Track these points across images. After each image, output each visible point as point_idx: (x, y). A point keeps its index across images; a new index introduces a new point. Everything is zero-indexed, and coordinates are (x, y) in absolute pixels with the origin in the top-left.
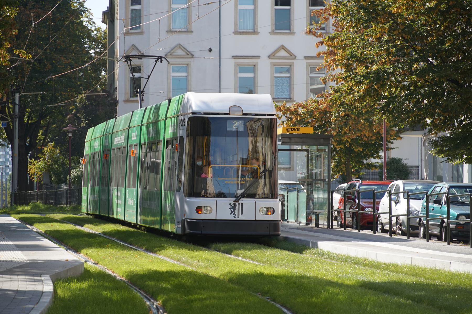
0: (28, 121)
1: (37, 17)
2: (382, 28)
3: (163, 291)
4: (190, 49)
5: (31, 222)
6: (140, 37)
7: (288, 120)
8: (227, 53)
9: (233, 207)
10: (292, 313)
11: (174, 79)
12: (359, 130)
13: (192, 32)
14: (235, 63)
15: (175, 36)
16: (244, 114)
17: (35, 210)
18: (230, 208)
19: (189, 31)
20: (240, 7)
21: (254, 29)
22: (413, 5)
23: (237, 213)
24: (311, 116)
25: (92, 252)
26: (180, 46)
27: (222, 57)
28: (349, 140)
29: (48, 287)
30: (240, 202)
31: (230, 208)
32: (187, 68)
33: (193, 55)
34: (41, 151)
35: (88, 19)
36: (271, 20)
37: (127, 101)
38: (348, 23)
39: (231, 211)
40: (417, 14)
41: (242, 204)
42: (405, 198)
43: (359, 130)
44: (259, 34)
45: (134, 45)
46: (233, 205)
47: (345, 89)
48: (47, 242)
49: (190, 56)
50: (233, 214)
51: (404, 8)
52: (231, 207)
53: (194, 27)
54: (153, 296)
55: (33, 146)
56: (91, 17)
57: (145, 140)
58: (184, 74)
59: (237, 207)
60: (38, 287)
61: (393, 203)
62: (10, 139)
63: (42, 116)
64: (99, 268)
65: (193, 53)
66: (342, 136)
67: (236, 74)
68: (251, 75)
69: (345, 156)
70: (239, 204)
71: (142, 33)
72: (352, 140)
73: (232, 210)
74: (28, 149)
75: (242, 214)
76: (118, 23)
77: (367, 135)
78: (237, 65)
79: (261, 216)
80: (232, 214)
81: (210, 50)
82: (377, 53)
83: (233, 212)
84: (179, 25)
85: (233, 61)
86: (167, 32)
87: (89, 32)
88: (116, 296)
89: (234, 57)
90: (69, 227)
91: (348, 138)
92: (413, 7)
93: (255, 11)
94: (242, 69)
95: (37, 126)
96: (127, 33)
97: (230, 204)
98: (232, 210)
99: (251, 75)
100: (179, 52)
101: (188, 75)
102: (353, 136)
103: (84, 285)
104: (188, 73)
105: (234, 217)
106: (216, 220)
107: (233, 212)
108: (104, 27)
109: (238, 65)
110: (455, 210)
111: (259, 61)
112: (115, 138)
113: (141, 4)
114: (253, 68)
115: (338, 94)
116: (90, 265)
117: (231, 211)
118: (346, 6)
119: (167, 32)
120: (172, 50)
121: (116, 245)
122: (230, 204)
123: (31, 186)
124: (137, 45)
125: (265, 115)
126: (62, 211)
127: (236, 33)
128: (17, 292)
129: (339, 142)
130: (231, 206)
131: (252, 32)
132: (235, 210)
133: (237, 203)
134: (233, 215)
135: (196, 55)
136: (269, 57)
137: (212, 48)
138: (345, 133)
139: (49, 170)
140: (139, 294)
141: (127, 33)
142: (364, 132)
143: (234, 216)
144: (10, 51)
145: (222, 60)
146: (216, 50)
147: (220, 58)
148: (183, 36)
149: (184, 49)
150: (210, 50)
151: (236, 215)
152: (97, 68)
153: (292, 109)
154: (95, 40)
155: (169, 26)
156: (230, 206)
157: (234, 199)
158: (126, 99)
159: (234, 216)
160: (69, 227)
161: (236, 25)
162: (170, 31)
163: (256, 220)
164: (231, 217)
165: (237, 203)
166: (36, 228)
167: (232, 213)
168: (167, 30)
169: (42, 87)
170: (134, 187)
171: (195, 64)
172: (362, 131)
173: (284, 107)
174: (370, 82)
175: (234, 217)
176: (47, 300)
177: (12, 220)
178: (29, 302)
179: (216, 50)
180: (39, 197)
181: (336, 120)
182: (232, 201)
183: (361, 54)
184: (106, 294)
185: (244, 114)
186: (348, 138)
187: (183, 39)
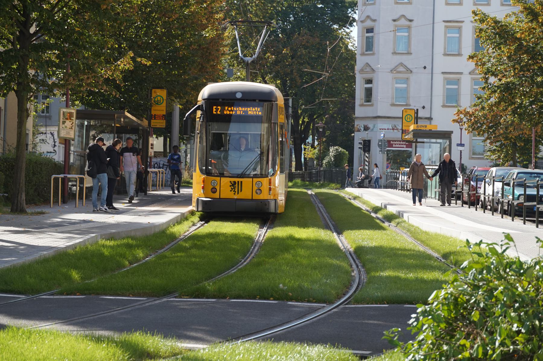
0: (316, 118)
1: (331, 43)
2: (509, 49)
4: (409, 66)
6: (372, 57)
7: (468, 121)
8: (437, 70)
11: (397, 89)
12: (521, 129)
13: (411, 54)
14: (444, 77)
15: (398, 57)
18: (230, 186)
19: (409, 53)
20: (448, 35)
21: (459, 52)
22: (534, 32)
23: (236, 190)
24: (485, 118)
26: (401, 64)
27: (434, 72)
28: (513, 137)
31: (230, 186)
32: (406, 81)
33: (411, 71)
35: (352, 45)
36: (472, 46)
37: (362, 105)
38: (488, 45)
40: (537, 38)
43: (521, 129)
44: (463, 56)
45: (367, 63)
47: (485, 96)
49: (409, 72)
51: (527, 34)
53: (413, 49)
56: (354, 43)
58: (405, 86)
59: (237, 185)
61: (487, 185)
65: (411, 69)
66: (508, 134)
67: (444, 86)
68: (456, 87)
69: (512, 149)
71: (373, 54)
72: (515, 137)
73: (232, 187)
75: (241, 191)
77: (527, 132)
78: (445, 79)
81: (425, 68)
82: (505, 68)
84: (401, 48)
85: (442, 76)
86: (392, 53)
89: (443, 73)
91: (513, 135)
92: (534, 33)
93: (460, 39)
94: (449, 82)
98: (232, 187)
99: (456, 87)
100: (401, 69)
101: (408, 86)
102: (516, 133)
104: (408, 85)
109: (446, 79)
110: (517, 191)
111: (462, 76)
114: (457, 82)
115: (480, 100)
118: (487, 32)
119: (392, 53)
120: (396, 67)
122: (230, 182)
124: (369, 63)
127: (445, 55)
129: (506, 138)
130: (231, 183)
131: (457, 54)
135: (414, 71)
136: (470, 73)
138: (511, 131)
142: (525, 131)
145: (434, 75)
146: (429, 68)
147: (432, 73)
148: (404, 57)
149: (405, 67)
150: (425, 68)
151: (235, 192)
153: (471, 113)
155: (394, 49)
156: (230, 184)
158: (361, 103)
161: (445, 48)
162: (394, 53)
168: (392, 52)
171: (413, 78)
172: (524, 130)
173: (465, 111)
174: (501, 91)
179: (429, 68)
181: (504, 122)
183: (495, 69)
186: (513, 135)
187: (404, 59)
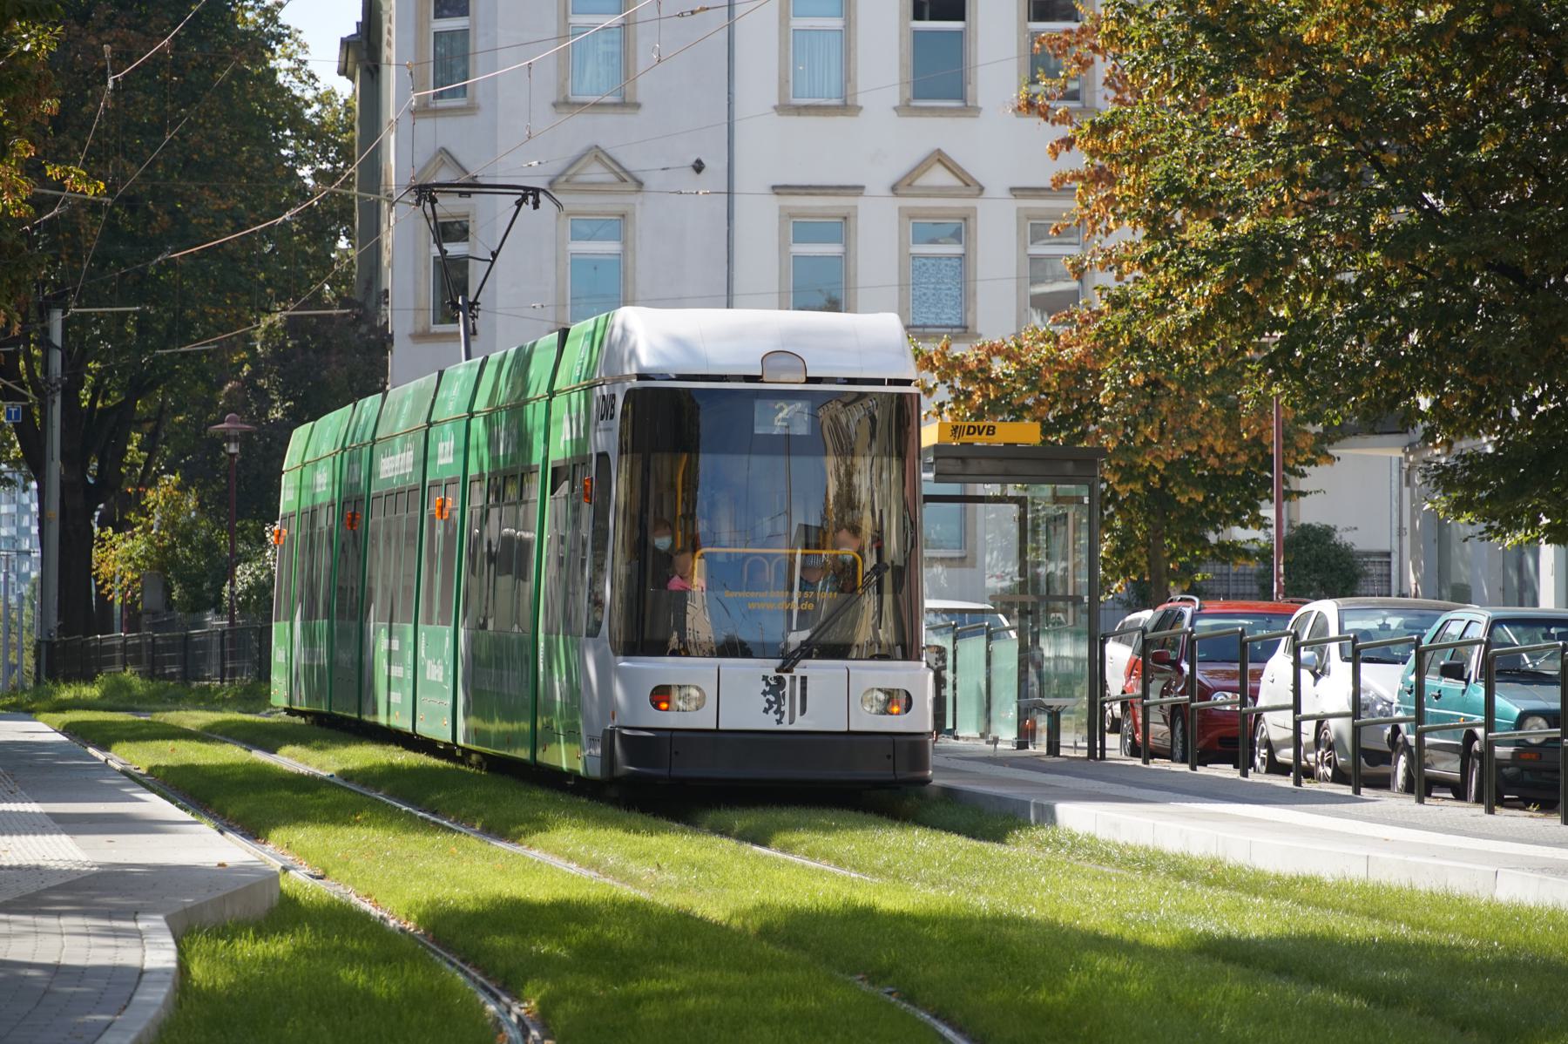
0: (93, 402)
1: (124, 57)
2: (1269, 92)
3: (542, 967)
4: (631, 162)
5: (105, 737)
6: (464, 122)
7: (956, 400)
8: (753, 177)
9: (775, 688)
10: (971, 1039)
11: (578, 262)
12: (1192, 433)
13: (637, 106)
14: (781, 208)
15: (581, 120)
16: (810, 380)
17: (117, 698)
18: (764, 693)
19: (627, 104)
20: (797, 23)
21: (844, 95)
22: (1373, 18)
23: (786, 708)
24: (1033, 386)
25: (307, 837)
26: (597, 154)
27: (737, 188)
28: (1160, 466)
29: (160, 954)
30: (798, 672)
31: (764, 693)
32: (620, 225)
33: (640, 184)
34: (135, 503)
35: (291, 64)
36: (902, 65)
37: (422, 336)
38: (1156, 75)
39: (768, 701)
40: (1386, 46)
41: (804, 679)
42: (1347, 660)
43: (1192, 433)
44: (862, 114)
45: (444, 151)
46: (772, 683)
47: (1145, 295)
48: (155, 805)
49: (632, 186)
50: (776, 712)
51: (1343, 26)
52: (767, 689)
53: (644, 89)
54: (509, 984)
55: (108, 485)
56: (301, 57)
57: (481, 465)
58: (612, 247)
59: (787, 689)
60: (127, 955)
61: (1306, 676)
62: (34, 463)
63: (139, 387)
64: (329, 891)
65: (641, 176)
66: (1137, 452)
67: (783, 248)
68: (834, 249)
69: (1146, 520)
70: (793, 679)
71: (471, 109)
72: (1168, 465)
73: (772, 698)
74: (93, 496)
75: (803, 710)
76: (391, 78)
77: (1219, 448)
78: (787, 215)
79: (867, 719)
80: (771, 712)
81: (699, 167)
82: (1251, 176)
83: (775, 706)
84: (593, 82)
85: (775, 201)
86: (555, 105)
87: (295, 106)
88: (384, 985)
89: (778, 190)
90: (230, 754)
91: (1157, 458)
92: (1373, 24)
93: (847, 37)
94: (802, 228)
95: (122, 420)
96: (422, 110)
97: (765, 678)
98: (772, 698)
99: (834, 249)
100: (596, 173)
101: (624, 251)
102: (1173, 451)
103: (280, 947)
104: (624, 243)
105: (779, 722)
106: (717, 731)
107: (775, 706)
108: (345, 88)
109: (791, 216)
110: (1510, 698)
111: (860, 202)
112: (383, 460)
113: (468, 15)
114: (841, 228)
115: (1124, 313)
116: (300, 882)
117: (768, 701)
118: (1151, 20)
119: (555, 105)
120: (571, 165)
121: (385, 816)
122: (765, 678)
123: (102, 617)
124: (454, 150)
125: (880, 382)
126: (207, 700)
127: (785, 108)
128: (56, 970)
129: (1128, 474)
130: (768, 684)
131: (837, 107)
132: (779, 699)
133: (787, 677)
134: (772, 716)
135: (651, 181)
136: (894, 189)
137: (704, 161)
138: (1147, 442)
139: (162, 565)
140: (460, 979)
141: (422, 110)
142: (1210, 439)
143: (778, 717)
144: (33, 169)
145: (737, 199)
146: (717, 165)
147: (730, 193)
148: (608, 120)
149: (612, 163)
150: (699, 167)
151: (782, 714)
152: (321, 225)
153: (972, 362)
154: (317, 134)
155: (562, 87)
156: (763, 686)
157: (778, 662)
158: (420, 329)
159: (778, 717)
160: (230, 754)
161: (783, 83)
162: (564, 104)
163: (849, 733)
164: (768, 722)
165: (787, 677)
166: (121, 756)
167: (771, 707)
168: (553, 98)
169: (140, 288)
170: (445, 623)
171: (647, 212)
172: (1203, 436)
173: (943, 354)
174: (1230, 272)
175: (779, 722)
176: (155, 998)
177: (41, 730)
178: (98, 1004)
179: (717, 165)
180: (131, 655)
181: (1115, 400)
182: (769, 667)
183: (1200, 180)
184: (353, 976)
185: (810, 380)
186: (1157, 458)
187: (608, 130)
